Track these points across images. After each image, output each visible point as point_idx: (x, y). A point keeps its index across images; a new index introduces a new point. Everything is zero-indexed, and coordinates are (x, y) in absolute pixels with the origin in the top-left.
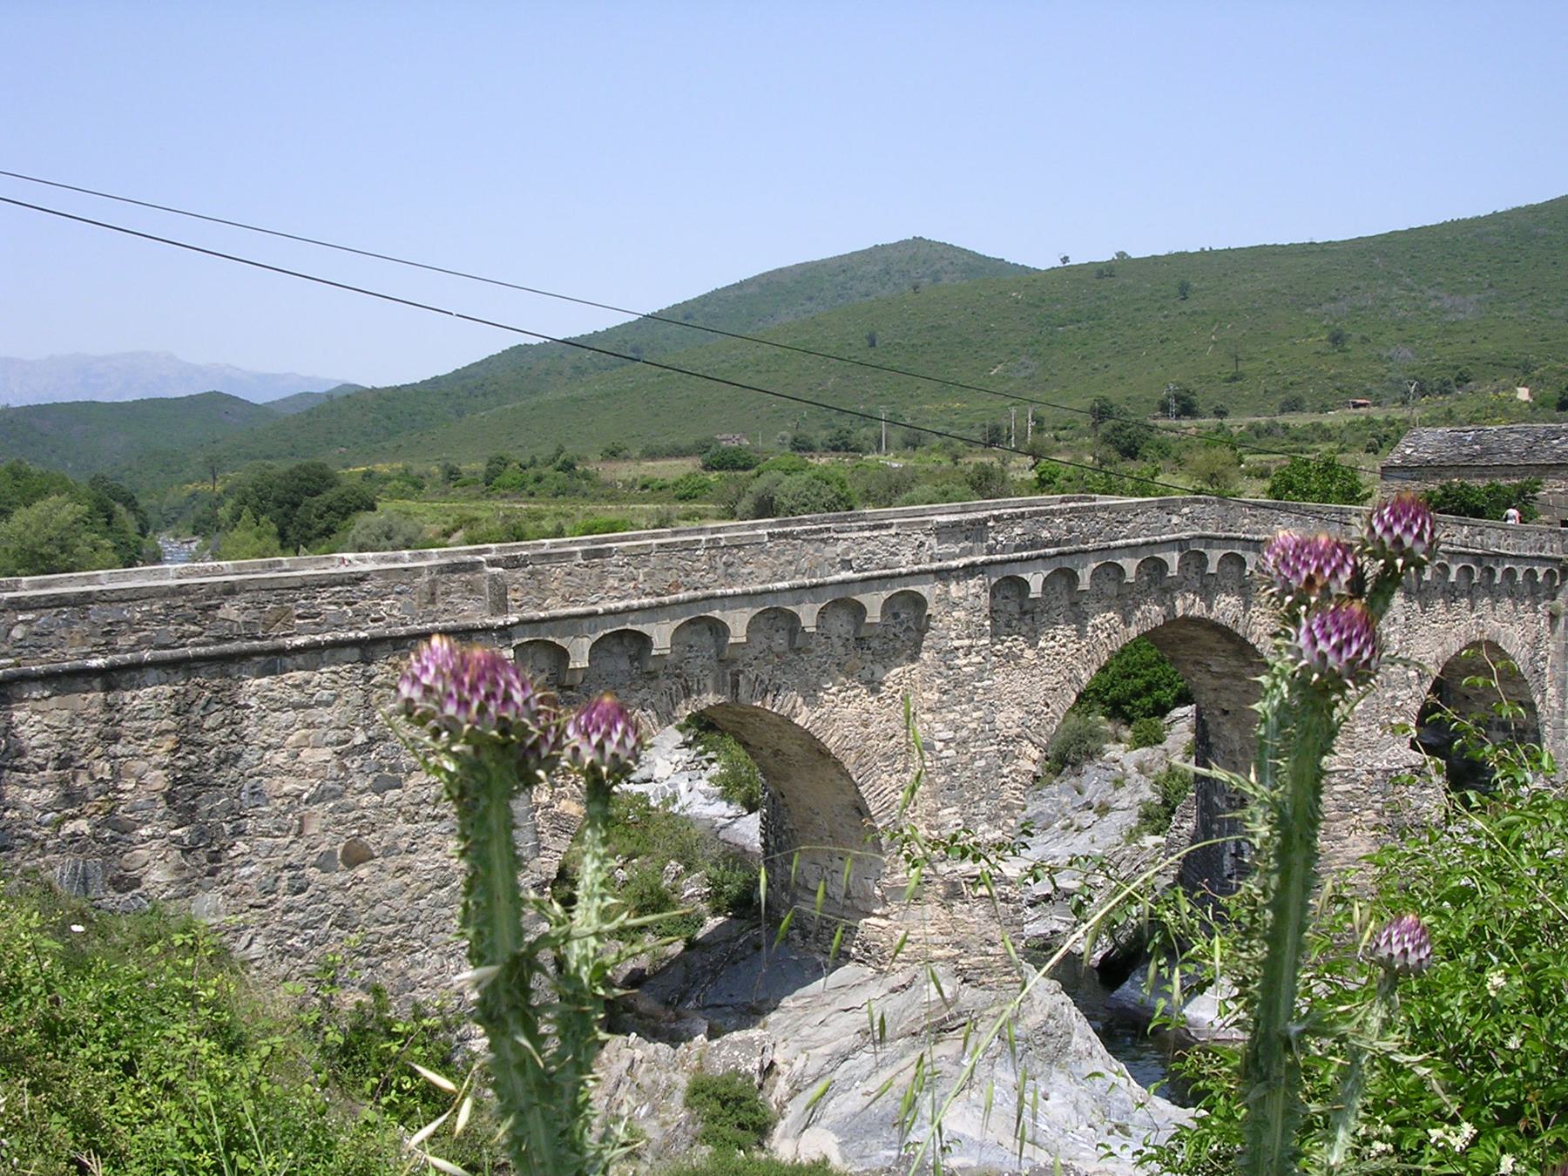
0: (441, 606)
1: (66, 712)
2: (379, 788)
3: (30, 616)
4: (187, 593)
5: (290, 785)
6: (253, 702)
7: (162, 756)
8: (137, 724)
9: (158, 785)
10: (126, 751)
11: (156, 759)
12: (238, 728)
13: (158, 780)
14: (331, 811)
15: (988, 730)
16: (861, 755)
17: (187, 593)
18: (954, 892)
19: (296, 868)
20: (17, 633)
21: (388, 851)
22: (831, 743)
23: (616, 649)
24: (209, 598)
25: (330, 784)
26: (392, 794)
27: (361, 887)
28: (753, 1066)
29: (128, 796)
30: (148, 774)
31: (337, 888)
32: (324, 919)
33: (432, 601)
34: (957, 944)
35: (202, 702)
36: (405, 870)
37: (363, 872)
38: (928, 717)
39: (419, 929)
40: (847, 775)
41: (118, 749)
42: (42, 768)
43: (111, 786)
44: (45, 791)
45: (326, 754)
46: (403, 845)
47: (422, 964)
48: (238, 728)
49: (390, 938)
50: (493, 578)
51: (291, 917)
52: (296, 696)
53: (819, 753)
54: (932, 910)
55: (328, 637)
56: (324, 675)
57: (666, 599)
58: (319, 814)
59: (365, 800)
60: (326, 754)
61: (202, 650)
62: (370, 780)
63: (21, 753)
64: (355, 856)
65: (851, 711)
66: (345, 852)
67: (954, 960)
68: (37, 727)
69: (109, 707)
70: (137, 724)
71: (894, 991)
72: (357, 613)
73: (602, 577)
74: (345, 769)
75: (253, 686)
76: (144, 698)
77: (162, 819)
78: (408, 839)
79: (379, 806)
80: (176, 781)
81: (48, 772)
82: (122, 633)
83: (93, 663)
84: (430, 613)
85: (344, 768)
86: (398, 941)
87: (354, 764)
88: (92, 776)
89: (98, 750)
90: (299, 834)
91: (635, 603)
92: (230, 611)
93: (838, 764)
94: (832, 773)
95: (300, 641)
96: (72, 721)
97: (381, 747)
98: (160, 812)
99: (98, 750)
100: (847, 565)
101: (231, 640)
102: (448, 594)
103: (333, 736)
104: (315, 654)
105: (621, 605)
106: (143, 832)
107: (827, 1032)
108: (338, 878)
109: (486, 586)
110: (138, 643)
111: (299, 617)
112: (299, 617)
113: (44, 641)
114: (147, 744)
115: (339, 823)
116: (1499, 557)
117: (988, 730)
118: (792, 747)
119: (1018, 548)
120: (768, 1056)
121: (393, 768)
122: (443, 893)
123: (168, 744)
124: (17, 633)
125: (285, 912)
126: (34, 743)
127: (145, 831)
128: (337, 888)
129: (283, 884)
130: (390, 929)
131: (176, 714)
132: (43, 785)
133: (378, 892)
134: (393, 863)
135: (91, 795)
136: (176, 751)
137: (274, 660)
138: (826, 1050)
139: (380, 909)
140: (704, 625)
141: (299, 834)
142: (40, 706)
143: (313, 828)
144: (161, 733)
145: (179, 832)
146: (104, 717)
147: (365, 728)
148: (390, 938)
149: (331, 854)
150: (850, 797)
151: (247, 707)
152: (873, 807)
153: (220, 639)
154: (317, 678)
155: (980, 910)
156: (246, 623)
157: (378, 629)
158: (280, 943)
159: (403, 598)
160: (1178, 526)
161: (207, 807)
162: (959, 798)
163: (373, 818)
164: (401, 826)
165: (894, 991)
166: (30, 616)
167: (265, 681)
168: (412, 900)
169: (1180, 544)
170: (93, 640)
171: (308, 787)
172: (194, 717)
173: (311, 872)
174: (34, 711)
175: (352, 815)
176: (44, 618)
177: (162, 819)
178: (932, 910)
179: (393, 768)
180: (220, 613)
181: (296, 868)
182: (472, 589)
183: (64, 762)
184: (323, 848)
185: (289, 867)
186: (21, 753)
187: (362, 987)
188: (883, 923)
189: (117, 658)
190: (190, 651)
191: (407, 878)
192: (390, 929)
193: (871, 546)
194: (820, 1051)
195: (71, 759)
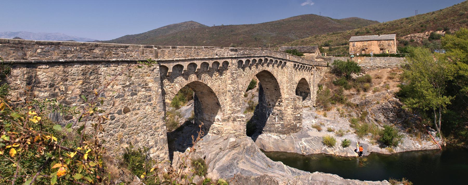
0: (145, 55)
1: (53, 73)
2: (132, 95)
3: (43, 47)
4: (86, 45)
5: (111, 94)
6: (103, 73)
7: (79, 85)
8: (72, 77)
9: (78, 93)
10: (69, 84)
11: (77, 86)
12: (99, 79)
13: (78, 91)
14: (121, 100)
15: (238, 89)
16: (219, 92)
17: (86, 45)
18: (234, 120)
19: (113, 114)
20: (39, 51)
21: (134, 109)
22: (214, 90)
23: (177, 69)
24: (92, 47)
25: (121, 94)
26: (135, 97)
27: (127, 118)
28: (203, 157)
29: (70, 95)
30: (75, 89)
31: (122, 119)
32: (118, 126)
33: (143, 54)
34: (235, 130)
35: (90, 72)
36: (137, 114)
37: (128, 114)
38: (229, 86)
39: (140, 128)
40: (216, 96)
41: (67, 83)
42: (45, 87)
43: (64, 93)
44: (46, 93)
45: (120, 87)
46: (137, 108)
47: (140, 136)
48: (99, 79)
49: (133, 130)
50: (155, 50)
51: (111, 126)
52: (113, 73)
53: (211, 92)
54: (231, 123)
55: (120, 59)
56: (120, 68)
57: (187, 59)
58: (118, 101)
59: (129, 98)
60: (120, 87)
61: (90, 60)
62: (130, 93)
63: (39, 83)
64: (126, 111)
65: (217, 84)
66: (124, 110)
67: (234, 133)
68: (44, 76)
69: (64, 72)
70: (72, 77)
71: (225, 140)
72: (127, 55)
73: (175, 53)
74: (125, 90)
75: (103, 69)
76: (75, 69)
77: (78, 101)
78: (138, 107)
79: (132, 99)
80: (82, 92)
81: (47, 88)
82: (68, 54)
83: (61, 60)
84: (143, 56)
85: (124, 90)
86: (135, 131)
87: (126, 89)
88: (59, 90)
89: (61, 83)
90: (113, 105)
91: (181, 59)
92: (97, 51)
93: (215, 94)
94: (213, 96)
95: (114, 60)
96: (54, 75)
97: (132, 86)
98: (78, 100)
99: (61, 83)
100: (217, 55)
101: (97, 58)
102: (146, 52)
103: (121, 83)
104: (117, 63)
105: (179, 59)
106: (73, 105)
107: (214, 149)
108: (121, 116)
109: (154, 51)
110: (73, 56)
111: (114, 54)
112: (114, 54)
113: (47, 53)
114: (75, 82)
115: (123, 103)
116: (305, 64)
117: (238, 89)
118: (205, 91)
119: (242, 55)
120: (205, 154)
121: (135, 91)
122: (145, 119)
123: (81, 82)
124: (39, 51)
125: (109, 125)
126: (43, 80)
127: (74, 104)
128: (122, 119)
129: (109, 118)
130: (134, 128)
131: (83, 75)
132: (46, 91)
133: (131, 119)
134: (134, 112)
135: (59, 95)
136: (83, 84)
137: (108, 63)
138: (214, 153)
139: (131, 123)
140: (192, 65)
141: (113, 105)
142: (45, 70)
143: (116, 105)
144: (79, 80)
145: (83, 105)
146: (63, 75)
147: (129, 81)
148: (133, 130)
149: (121, 110)
150: (216, 101)
151: (101, 74)
152: (221, 103)
153: (94, 57)
154: (118, 69)
155: (239, 123)
156: (100, 54)
157: (132, 59)
158: (108, 133)
159: (137, 53)
160: (264, 53)
161: (90, 99)
162: (235, 101)
163: (131, 102)
164: (137, 104)
165: (225, 140)
166: (43, 47)
167: (105, 68)
168: (138, 121)
169: (264, 57)
170: (61, 54)
171: (116, 94)
172: (87, 76)
173: (116, 115)
174: (43, 72)
175: (126, 101)
176: (47, 48)
177: (78, 101)
178: (231, 123)
179: (135, 91)
180: (94, 51)
181: (113, 114)
182: (151, 52)
183: (51, 86)
184: (119, 109)
185: (111, 113)
186: (39, 83)
187: (127, 143)
188: (222, 126)
189: (67, 60)
190: (87, 60)
191: (137, 116)
192: (134, 128)
193: (221, 51)
194: (213, 153)
195: (54, 85)
